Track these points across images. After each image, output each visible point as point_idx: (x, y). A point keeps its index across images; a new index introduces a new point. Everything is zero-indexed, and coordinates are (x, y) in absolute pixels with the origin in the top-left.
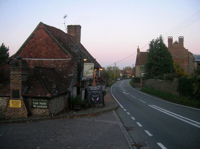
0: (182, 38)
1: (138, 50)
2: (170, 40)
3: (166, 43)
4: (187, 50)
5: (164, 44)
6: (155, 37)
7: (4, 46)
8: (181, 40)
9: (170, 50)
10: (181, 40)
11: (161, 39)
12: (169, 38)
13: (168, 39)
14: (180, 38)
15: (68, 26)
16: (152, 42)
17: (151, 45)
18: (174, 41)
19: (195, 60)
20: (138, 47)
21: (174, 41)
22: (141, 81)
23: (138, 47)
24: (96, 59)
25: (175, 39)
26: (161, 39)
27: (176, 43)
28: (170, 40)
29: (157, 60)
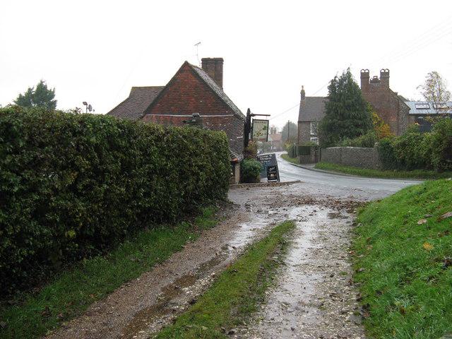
0: (387, 71)
1: (303, 93)
2: (365, 76)
3: (357, 80)
4: (396, 94)
5: (354, 83)
6: (338, 72)
7: (45, 87)
8: (385, 75)
9: (364, 96)
10: (385, 75)
11: (348, 76)
12: (363, 71)
13: (361, 73)
14: (383, 71)
15: (203, 60)
16: (333, 81)
17: (332, 88)
18: (371, 77)
19: (411, 112)
20: (303, 87)
21: (371, 77)
22: (313, 152)
23: (303, 87)
24: (42, 95)
25: (375, 73)
26: (348, 76)
27: (375, 80)
28: (365, 76)
29: (343, 117)
